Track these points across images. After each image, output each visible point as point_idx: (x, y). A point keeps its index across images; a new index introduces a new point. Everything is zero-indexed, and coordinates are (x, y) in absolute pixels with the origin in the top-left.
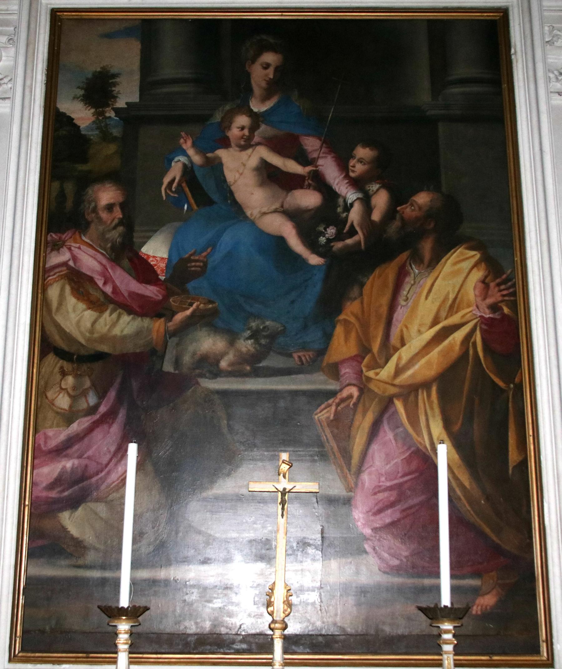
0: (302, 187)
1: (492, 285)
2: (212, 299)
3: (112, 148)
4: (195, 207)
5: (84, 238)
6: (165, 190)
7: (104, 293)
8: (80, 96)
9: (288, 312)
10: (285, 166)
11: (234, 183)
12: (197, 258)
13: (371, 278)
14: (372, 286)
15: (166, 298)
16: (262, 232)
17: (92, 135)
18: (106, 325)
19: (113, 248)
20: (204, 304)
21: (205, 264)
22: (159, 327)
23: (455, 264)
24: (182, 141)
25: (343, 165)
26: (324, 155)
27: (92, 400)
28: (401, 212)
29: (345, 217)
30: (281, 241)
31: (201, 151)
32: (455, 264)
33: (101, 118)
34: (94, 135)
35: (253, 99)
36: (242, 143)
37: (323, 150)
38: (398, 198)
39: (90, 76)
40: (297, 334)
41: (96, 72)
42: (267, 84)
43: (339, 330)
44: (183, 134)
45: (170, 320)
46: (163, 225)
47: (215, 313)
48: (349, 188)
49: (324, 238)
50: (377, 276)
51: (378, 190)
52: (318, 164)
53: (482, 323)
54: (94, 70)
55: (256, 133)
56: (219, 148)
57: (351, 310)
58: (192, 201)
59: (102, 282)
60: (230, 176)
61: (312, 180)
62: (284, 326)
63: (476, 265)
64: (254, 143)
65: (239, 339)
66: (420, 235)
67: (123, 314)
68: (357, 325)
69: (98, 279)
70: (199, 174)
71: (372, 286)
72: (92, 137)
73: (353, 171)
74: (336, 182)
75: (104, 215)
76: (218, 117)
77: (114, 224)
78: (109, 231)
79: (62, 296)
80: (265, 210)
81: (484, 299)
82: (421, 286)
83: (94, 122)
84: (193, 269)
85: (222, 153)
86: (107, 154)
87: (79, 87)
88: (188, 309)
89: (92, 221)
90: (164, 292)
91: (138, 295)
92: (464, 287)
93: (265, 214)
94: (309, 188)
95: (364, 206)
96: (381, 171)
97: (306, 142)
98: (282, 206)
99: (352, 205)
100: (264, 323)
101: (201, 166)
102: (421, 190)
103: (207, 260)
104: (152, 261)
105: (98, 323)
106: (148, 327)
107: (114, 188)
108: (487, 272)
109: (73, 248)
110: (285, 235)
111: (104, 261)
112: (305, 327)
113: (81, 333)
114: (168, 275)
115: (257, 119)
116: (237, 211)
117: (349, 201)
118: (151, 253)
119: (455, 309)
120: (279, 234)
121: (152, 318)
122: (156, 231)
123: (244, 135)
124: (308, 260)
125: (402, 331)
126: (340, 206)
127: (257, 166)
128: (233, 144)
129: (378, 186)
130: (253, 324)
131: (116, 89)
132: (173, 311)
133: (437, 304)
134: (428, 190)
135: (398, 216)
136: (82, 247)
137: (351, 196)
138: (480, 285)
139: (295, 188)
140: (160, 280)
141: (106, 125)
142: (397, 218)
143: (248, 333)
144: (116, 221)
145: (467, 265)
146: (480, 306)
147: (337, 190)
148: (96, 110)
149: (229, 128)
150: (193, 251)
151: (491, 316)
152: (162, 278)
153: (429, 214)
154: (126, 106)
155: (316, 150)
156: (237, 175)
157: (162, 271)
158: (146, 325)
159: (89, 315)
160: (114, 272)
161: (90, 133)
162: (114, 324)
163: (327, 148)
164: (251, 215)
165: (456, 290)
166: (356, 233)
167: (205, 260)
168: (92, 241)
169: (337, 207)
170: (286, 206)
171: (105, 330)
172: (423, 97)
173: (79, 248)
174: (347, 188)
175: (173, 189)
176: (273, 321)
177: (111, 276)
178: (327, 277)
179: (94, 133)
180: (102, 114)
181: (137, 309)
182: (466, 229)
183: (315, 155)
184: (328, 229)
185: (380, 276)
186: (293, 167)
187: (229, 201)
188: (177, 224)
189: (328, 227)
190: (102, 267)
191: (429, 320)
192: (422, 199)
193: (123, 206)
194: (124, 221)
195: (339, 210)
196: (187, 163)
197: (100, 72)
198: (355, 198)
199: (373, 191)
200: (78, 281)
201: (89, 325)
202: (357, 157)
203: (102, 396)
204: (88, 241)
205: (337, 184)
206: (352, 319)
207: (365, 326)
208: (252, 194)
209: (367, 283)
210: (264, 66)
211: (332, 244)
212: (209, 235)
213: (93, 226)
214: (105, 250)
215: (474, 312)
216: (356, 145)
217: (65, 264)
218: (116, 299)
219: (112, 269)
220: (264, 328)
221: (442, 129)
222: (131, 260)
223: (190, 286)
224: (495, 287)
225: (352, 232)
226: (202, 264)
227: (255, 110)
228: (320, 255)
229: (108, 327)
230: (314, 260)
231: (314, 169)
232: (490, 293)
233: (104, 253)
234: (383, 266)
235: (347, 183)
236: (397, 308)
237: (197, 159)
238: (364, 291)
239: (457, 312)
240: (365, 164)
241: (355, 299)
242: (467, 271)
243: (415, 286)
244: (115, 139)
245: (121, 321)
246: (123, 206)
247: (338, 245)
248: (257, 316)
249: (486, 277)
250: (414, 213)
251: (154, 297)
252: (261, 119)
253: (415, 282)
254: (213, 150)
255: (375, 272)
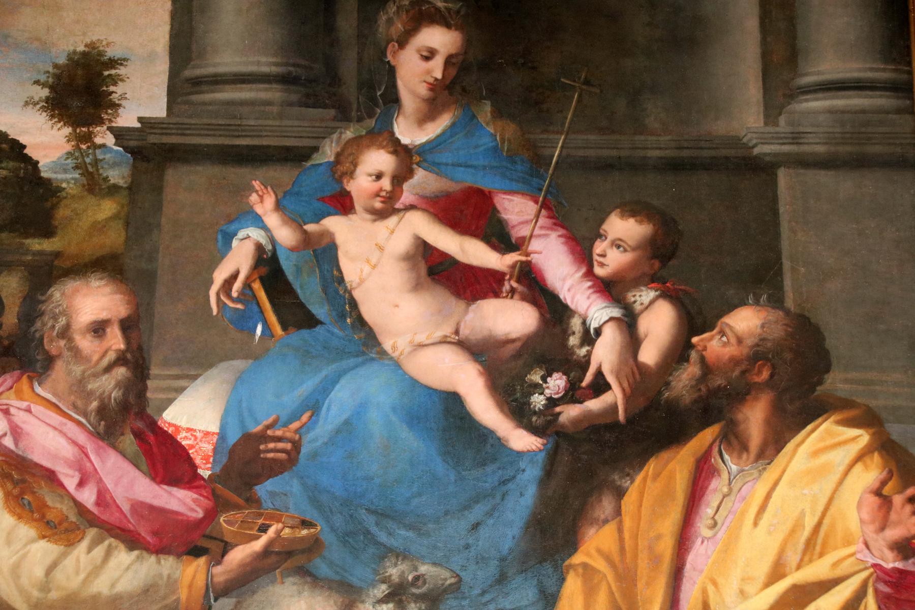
0: (497, 295)
1: (898, 500)
2: (308, 518)
3: (108, 208)
4: (278, 329)
5: (38, 390)
6: (218, 294)
7: (78, 505)
8: (41, 100)
9: (467, 547)
10: (463, 250)
11: (359, 285)
12: (279, 433)
13: (639, 478)
14: (641, 494)
15: (211, 515)
16: (414, 383)
17: (62, 181)
18: (77, 573)
19: (102, 411)
20: (292, 527)
21: (297, 446)
22: (194, 577)
23: (816, 453)
24: (254, 198)
25: (582, 251)
26: (543, 232)
28: (700, 348)
29: (585, 356)
30: (452, 403)
31: (295, 220)
32: (816, 453)
33: (84, 147)
34: (68, 180)
35: (401, 119)
36: (378, 204)
37: (542, 221)
38: (695, 320)
39: (62, 60)
40: (484, 592)
41: (75, 52)
42: (431, 90)
43: (572, 586)
44: (256, 184)
45: (219, 563)
46: (211, 366)
47: (314, 546)
48: (594, 296)
49: (542, 397)
50: (650, 473)
51: (652, 302)
52: (531, 248)
53: (878, 579)
54: (71, 48)
55: (406, 186)
56: (329, 214)
57: (597, 544)
58: (272, 318)
59: (76, 480)
60: (350, 270)
61: (518, 281)
62: (458, 575)
63: (860, 458)
64: (401, 207)
65: (363, 602)
66: (739, 394)
67: (116, 547)
68: (610, 577)
69: (67, 475)
70: (287, 265)
71: (641, 494)
72: (64, 185)
73: (602, 265)
74: (566, 287)
75: (86, 344)
76: (329, 152)
77: (105, 362)
78: (96, 375)
80: (422, 338)
81: (882, 528)
82: (744, 499)
83: (69, 154)
84: (270, 455)
85: (335, 224)
86: (92, 221)
87: (37, 82)
88: (257, 538)
89: (59, 356)
90: (206, 501)
91: (152, 508)
92: (836, 503)
93: (422, 346)
94: (512, 297)
95: (626, 336)
96: (661, 261)
97: (506, 203)
98: (457, 332)
99: (598, 332)
100: (416, 569)
101: (292, 249)
102: (742, 303)
103: (300, 438)
104: (186, 438)
105: (60, 567)
106: (169, 577)
107: (108, 289)
108: (885, 473)
109: (13, 411)
110: (462, 390)
111: (82, 438)
112: (502, 579)
113: (21, 591)
114: (218, 469)
115: (408, 158)
116: (364, 339)
117: (594, 325)
118: (183, 422)
119: (818, 548)
120: (450, 388)
121: (179, 556)
122: (195, 378)
123: (381, 190)
124: (507, 441)
125: (704, 592)
126: (574, 333)
127: (407, 253)
128: (358, 206)
129: (652, 294)
130: (394, 571)
131: (118, 90)
132: (226, 543)
133: (779, 537)
134: (757, 302)
135: (694, 355)
136: (34, 408)
137: (597, 311)
138: (874, 500)
139: (484, 296)
140: (202, 478)
141: (96, 162)
142: (692, 361)
143: (382, 590)
144: (111, 356)
145: (842, 457)
146: (872, 544)
147: (569, 302)
148: (75, 131)
149: (351, 174)
150: (270, 420)
151: (899, 565)
152: (205, 473)
153: (759, 354)
154: (138, 125)
155: (526, 222)
156: (367, 269)
157: (206, 458)
158: (165, 573)
159: (44, 551)
160: (103, 462)
161: (60, 176)
162: (96, 571)
163: (549, 217)
164: (394, 348)
165: (820, 508)
166: (607, 387)
167: (297, 437)
168: (55, 395)
169: (569, 336)
170: (465, 332)
171: (74, 583)
172: (744, 114)
173: (28, 410)
174: (588, 298)
175: (235, 294)
176: (434, 564)
177: (96, 470)
178: (549, 472)
179: (69, 176)
180: (87, 138)
181: (149, 538)
182: (835, 382)
183: (525, 232)
184: (549, 379)
185: (656, 476)
186: (475, 253)
187: (348, 320)
188: (239, 364)
189: (550, 375)
190: (76, 449)
191: (763, 569)
192: (746, 321)
193: (127, 326)
194: (129, 356)
195: (573, 341)
196: (263, 241)
197: (84, 54)
198: (607, 318)
199: (642, 304)
201: (39, 572)
202: (610, 237)
204: (49, 396)
205: (569, 290)
206: (600, 564)
207: (627, 578)
208: (397, 306)
209: (630, 490)
210: (425, 54)
211: (558, 409)
212: (309, 385)
213: (59, 366)
214: (85, 415)
215: (859, 556)
216: (608, 214)
218: (104, 517)
219: (98, 454)
220: (417, 578)
221: (783, 177)
222: (138, 435)
223: (263, 490)
224: (903, 506)
225: (600, 386)
226: (289, 446)
227: (405, 140)
228: (535, 431)
229: (82, 576)
230: (521, 440)
231: (524, 258)
232: (893, 516)
233: (83, 421)
234: (665, 455)
235: (590, 287)
236: (694, 542)
237: (285, 235)
238: (623, 507)
239: (821, 555)
240: (625, 251)
241: (606, 521)
242: (842, 468)
243: (732, 497)
244: (114, 190)
245: (113, 563)
246: (127, 326)
247: (570, 413)
248: (402, 555)
249: (884, 483)
250: (727, 350)
251: (190, 514)
252: (416, 158)
253: (730, 490)
254: (318, 218)
255: (646, 468)
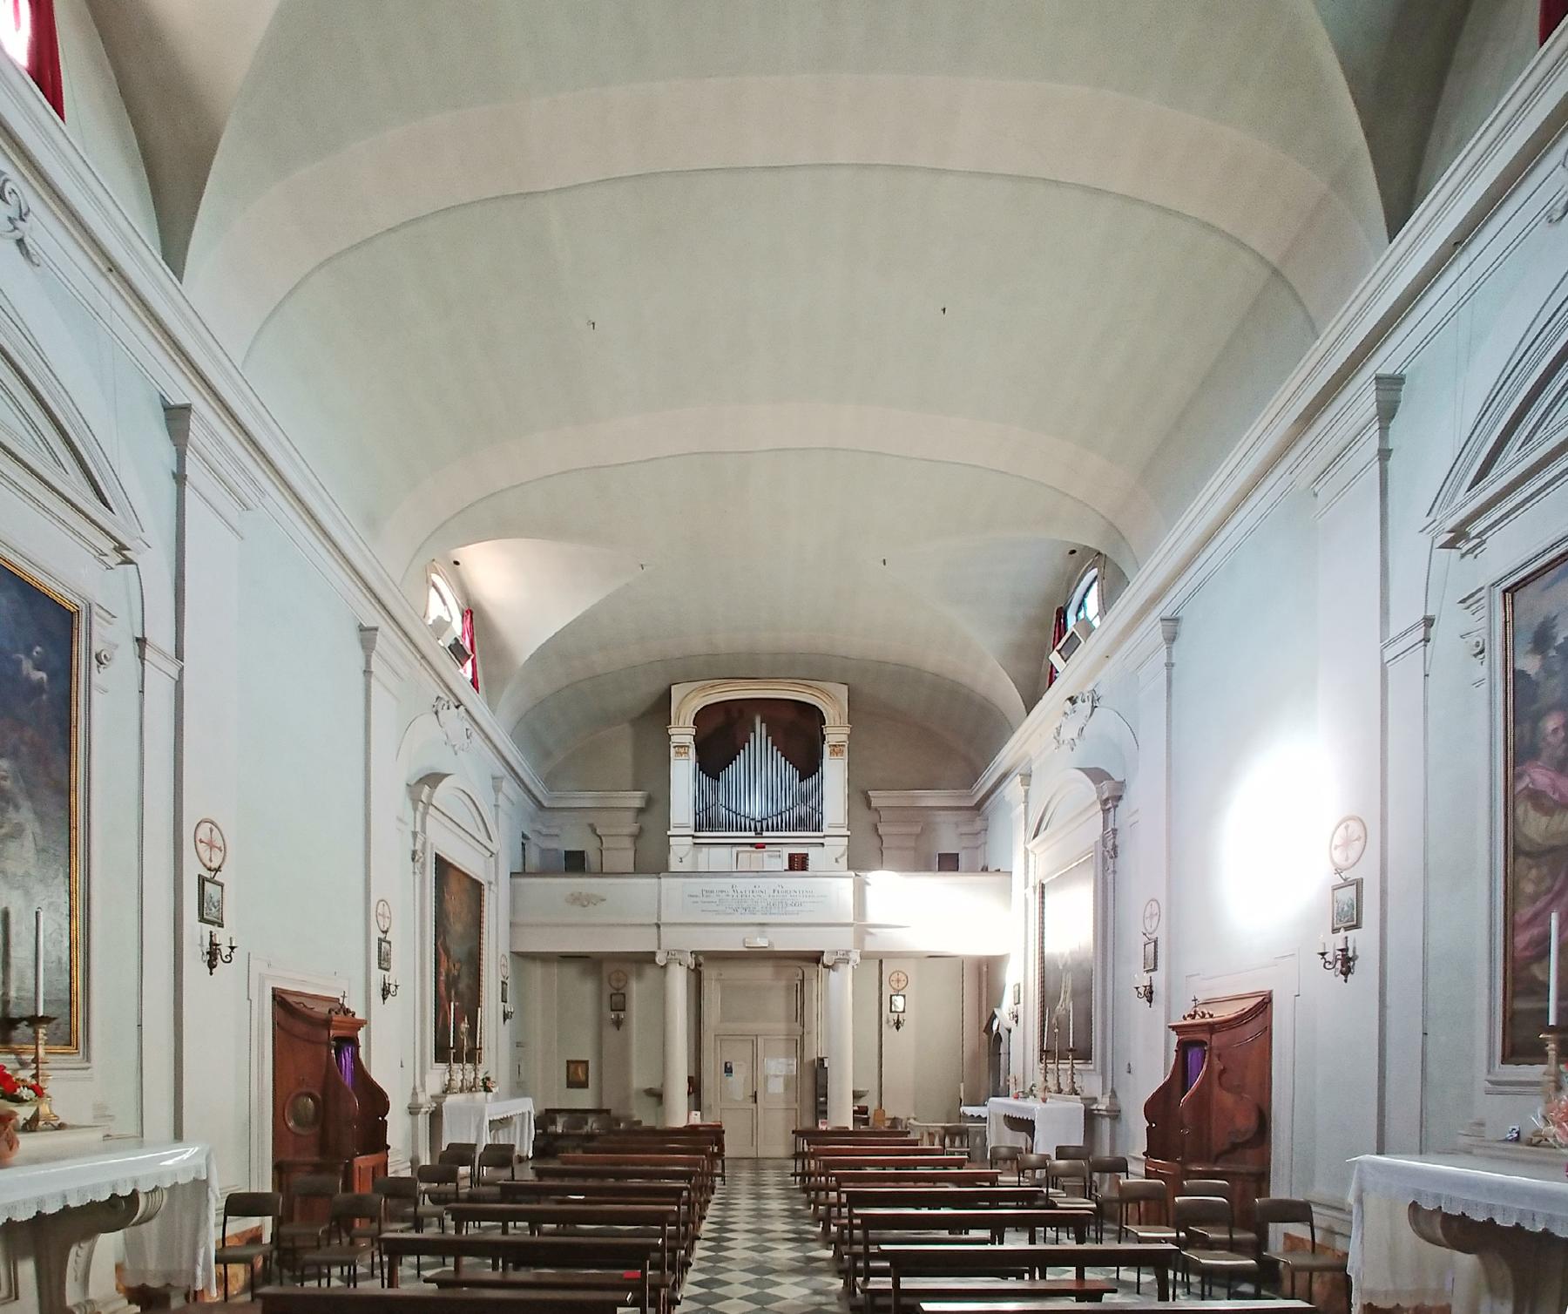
27: (1548, 882)
75: (1550, 739)
79: (1526, 811)
159: (1544, 820)
200: (1536, 798)
203: (1555, 877)
217: (1527, 787)
